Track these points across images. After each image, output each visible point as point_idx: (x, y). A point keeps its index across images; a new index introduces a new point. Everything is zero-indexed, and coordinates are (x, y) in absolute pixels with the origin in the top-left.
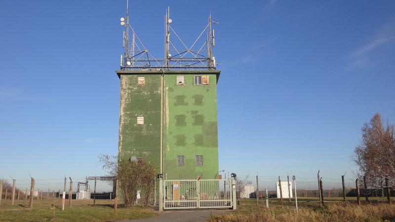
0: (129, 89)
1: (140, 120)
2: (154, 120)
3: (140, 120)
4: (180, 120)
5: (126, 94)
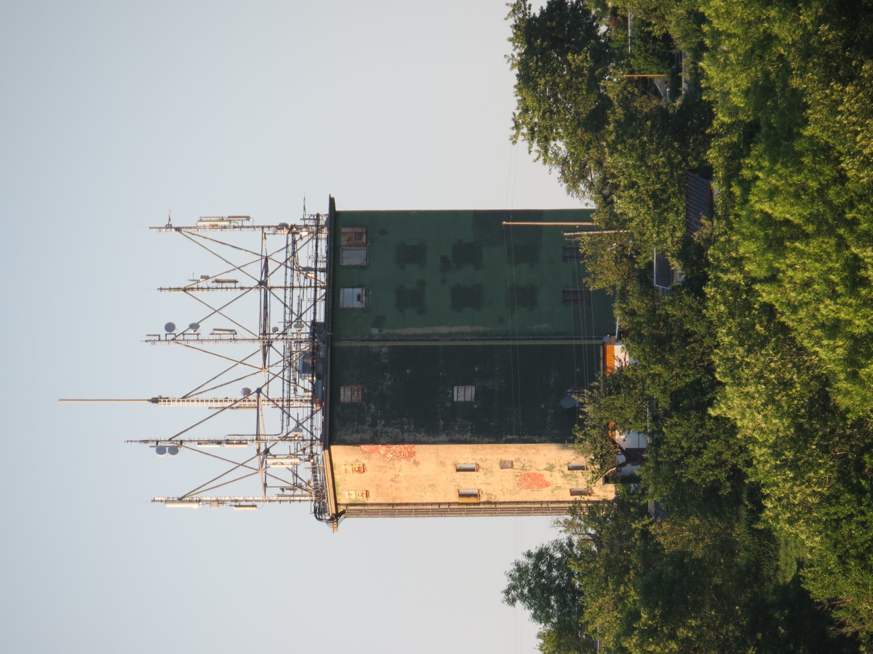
0: (374, 424)
1: (464, 394)
2: (463, 362)
3: (464, 394)
4: (466, 299)
5: (390, 430)
